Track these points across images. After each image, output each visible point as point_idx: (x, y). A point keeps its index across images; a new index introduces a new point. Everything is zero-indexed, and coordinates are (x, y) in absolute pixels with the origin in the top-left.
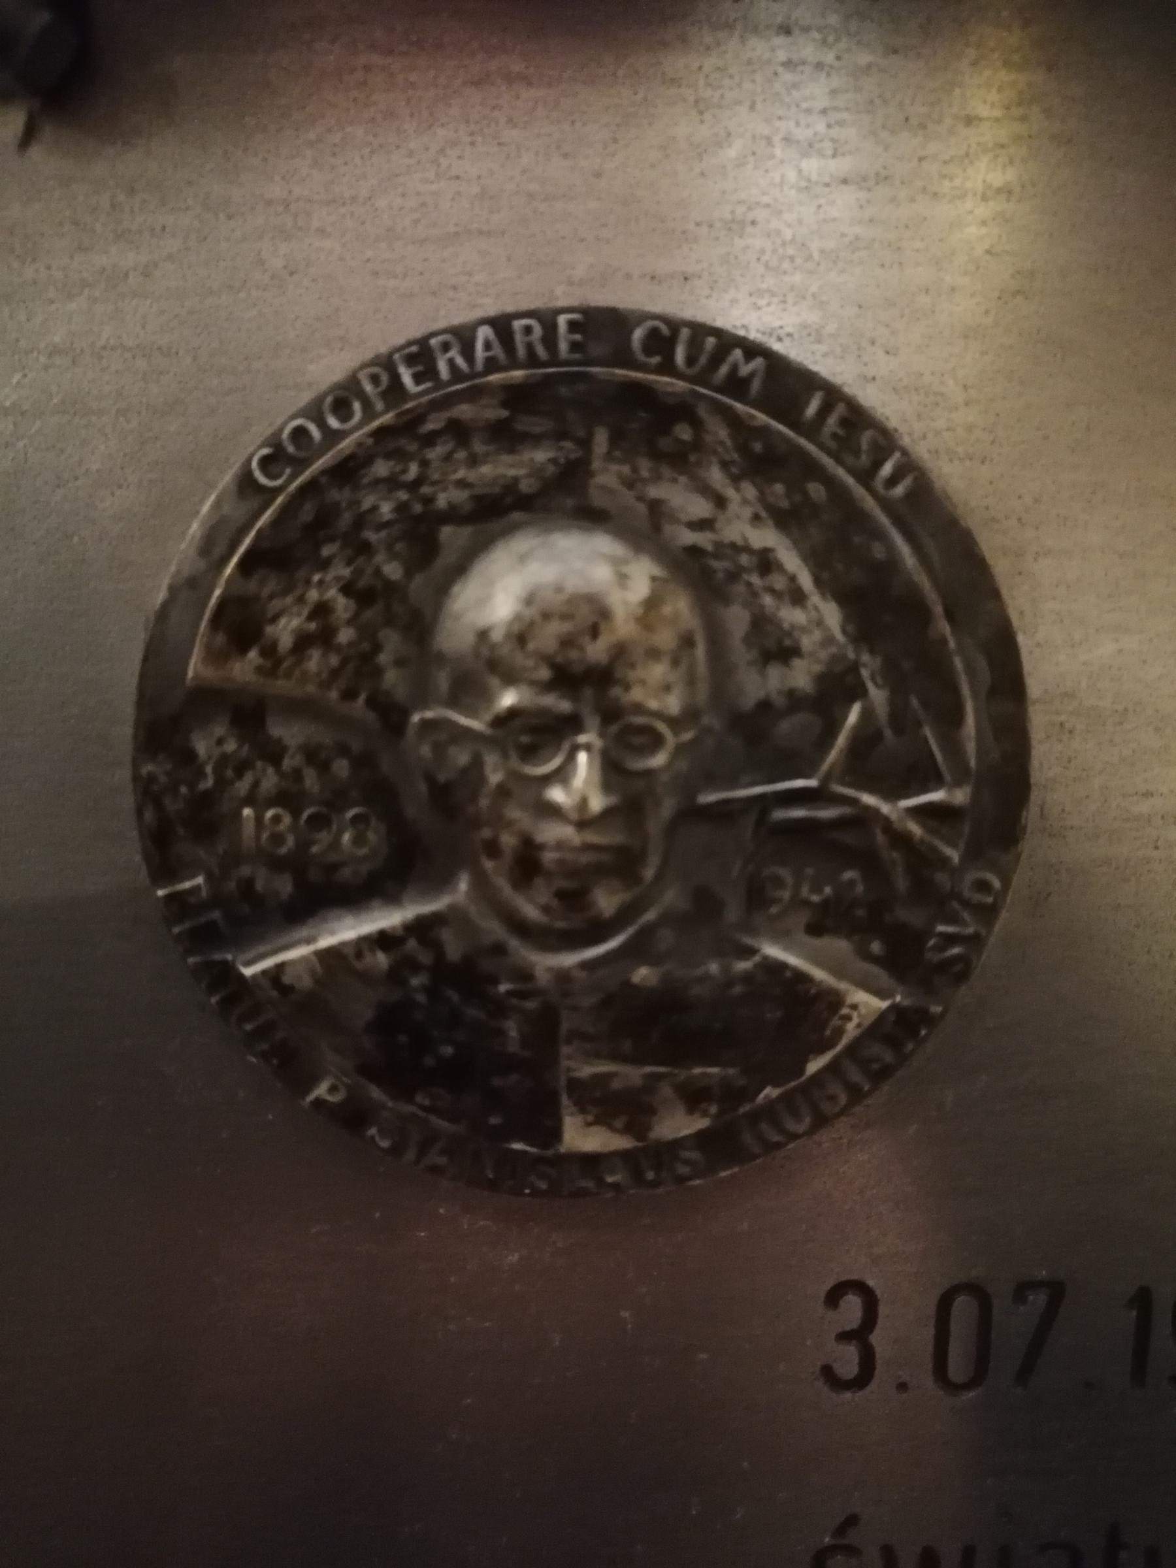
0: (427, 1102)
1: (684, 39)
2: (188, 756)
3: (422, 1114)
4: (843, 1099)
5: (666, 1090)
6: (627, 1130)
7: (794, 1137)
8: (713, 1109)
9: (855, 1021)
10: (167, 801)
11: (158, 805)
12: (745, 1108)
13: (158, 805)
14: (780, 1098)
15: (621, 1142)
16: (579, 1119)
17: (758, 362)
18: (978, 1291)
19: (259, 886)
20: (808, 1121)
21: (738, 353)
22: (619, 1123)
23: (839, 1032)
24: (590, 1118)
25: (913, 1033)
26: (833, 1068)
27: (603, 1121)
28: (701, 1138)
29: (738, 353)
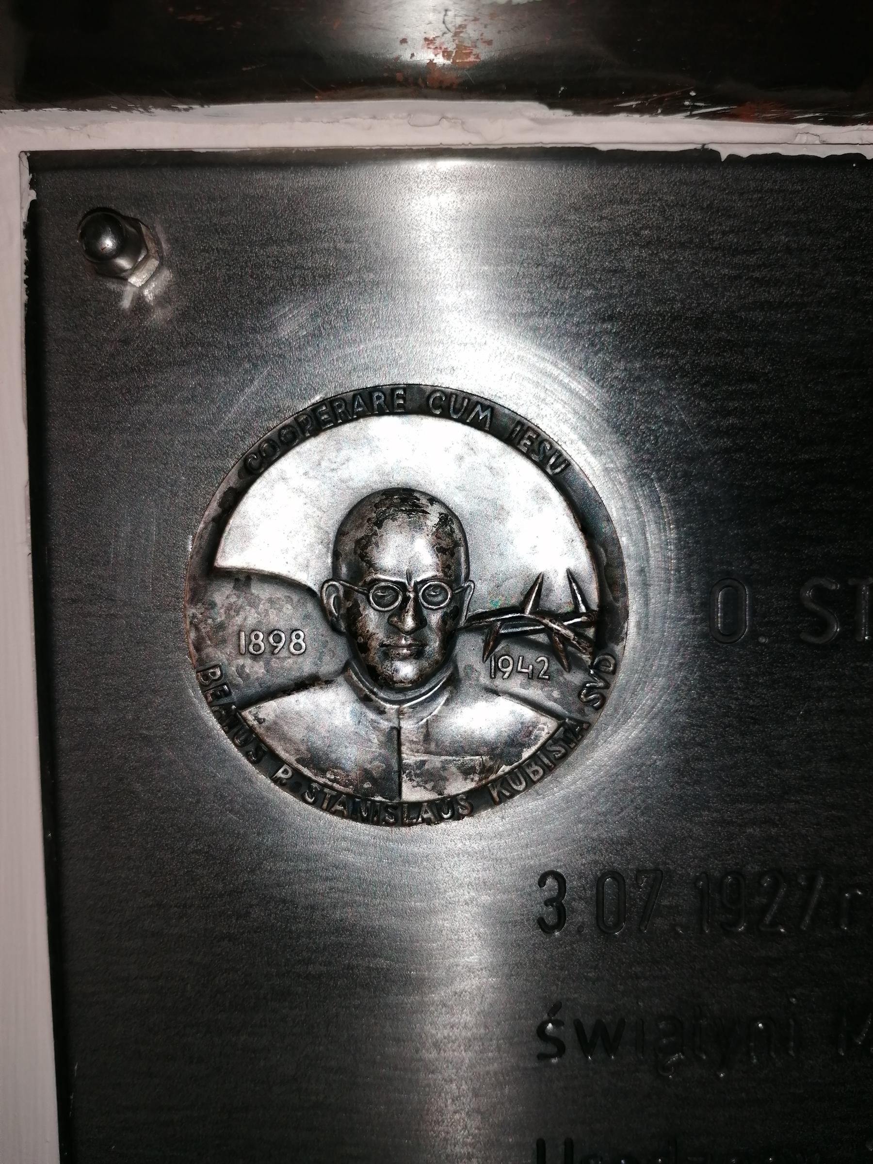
0: (333, 777)
1: (146, 109)
2: (213, 605)
3: (330, 783)
4: (541, 772)
5: (454, 769)
6: (433, 788)
7: (519, 792)
8: (477, 778)
9: (546, 731)
10: (202, 626)
11: (197, 629)
12: (493, 777)
13: (197, 629)
14: (509, 773)
15: (433, 796)
16: (410, 784)
17: (488, 413)
18: (615, 875)
19: (247, 670)
20: (524, 784)
21: (478, 408)
22: (429, 786)
23: (537, 738)
24: (415, 784)
25: (600, 1027)
26: (533, 757)
27: (422, 785)
28: (470, 794)
29: (478, 408)
